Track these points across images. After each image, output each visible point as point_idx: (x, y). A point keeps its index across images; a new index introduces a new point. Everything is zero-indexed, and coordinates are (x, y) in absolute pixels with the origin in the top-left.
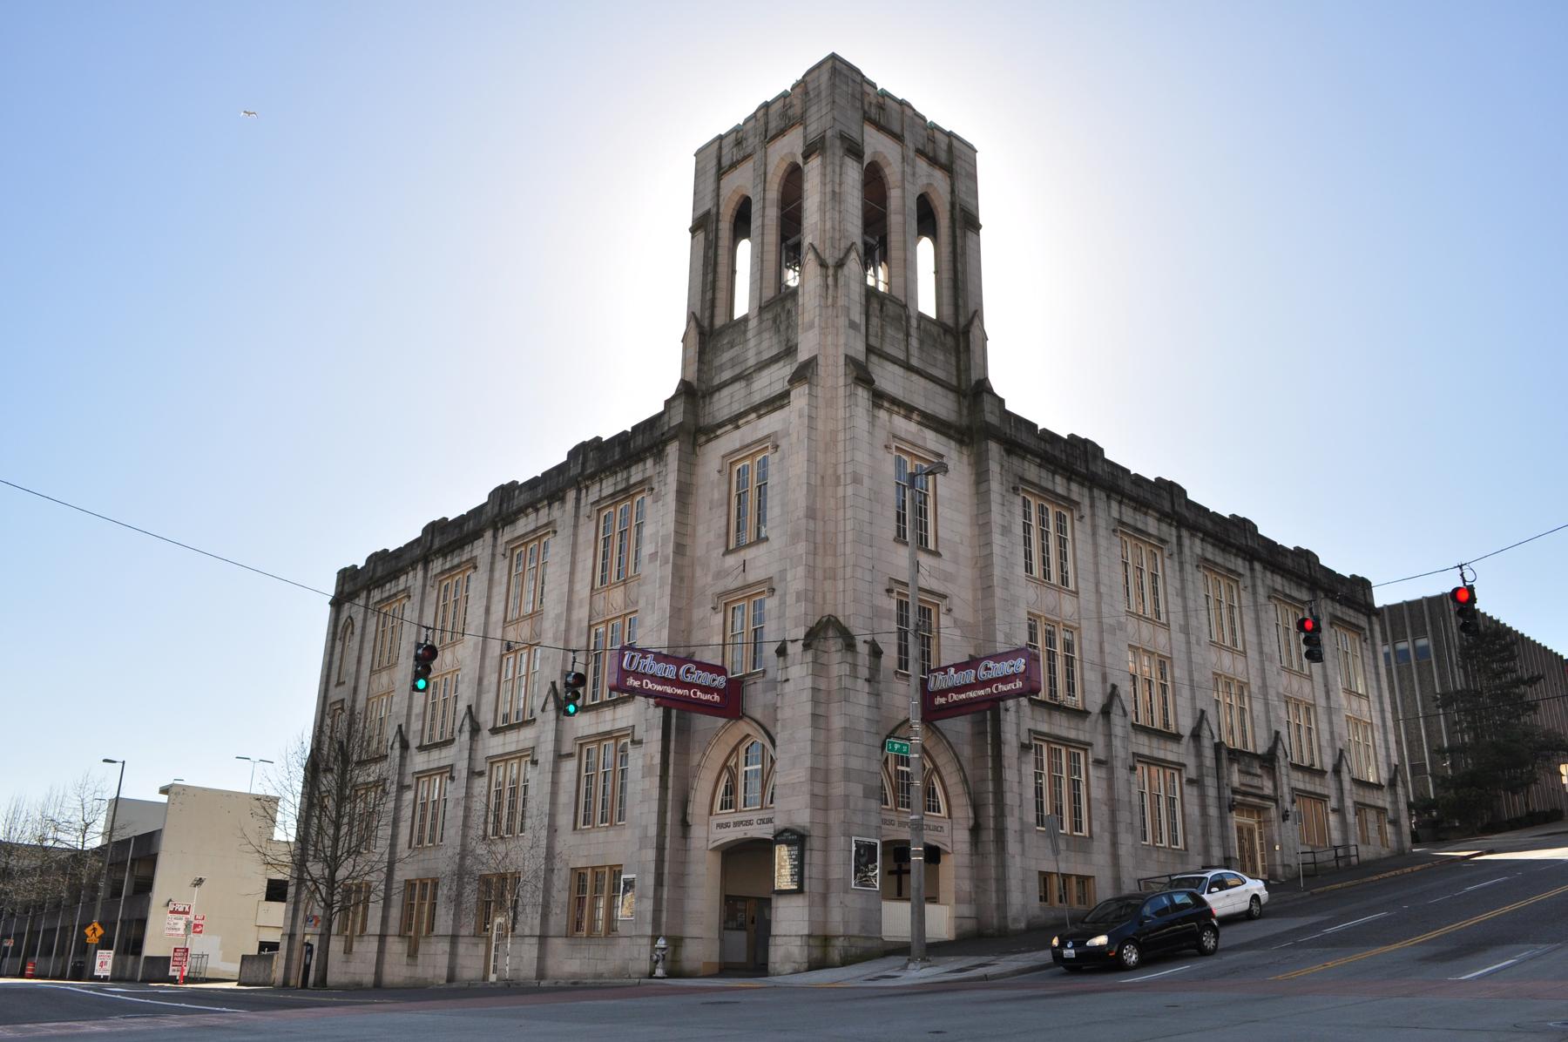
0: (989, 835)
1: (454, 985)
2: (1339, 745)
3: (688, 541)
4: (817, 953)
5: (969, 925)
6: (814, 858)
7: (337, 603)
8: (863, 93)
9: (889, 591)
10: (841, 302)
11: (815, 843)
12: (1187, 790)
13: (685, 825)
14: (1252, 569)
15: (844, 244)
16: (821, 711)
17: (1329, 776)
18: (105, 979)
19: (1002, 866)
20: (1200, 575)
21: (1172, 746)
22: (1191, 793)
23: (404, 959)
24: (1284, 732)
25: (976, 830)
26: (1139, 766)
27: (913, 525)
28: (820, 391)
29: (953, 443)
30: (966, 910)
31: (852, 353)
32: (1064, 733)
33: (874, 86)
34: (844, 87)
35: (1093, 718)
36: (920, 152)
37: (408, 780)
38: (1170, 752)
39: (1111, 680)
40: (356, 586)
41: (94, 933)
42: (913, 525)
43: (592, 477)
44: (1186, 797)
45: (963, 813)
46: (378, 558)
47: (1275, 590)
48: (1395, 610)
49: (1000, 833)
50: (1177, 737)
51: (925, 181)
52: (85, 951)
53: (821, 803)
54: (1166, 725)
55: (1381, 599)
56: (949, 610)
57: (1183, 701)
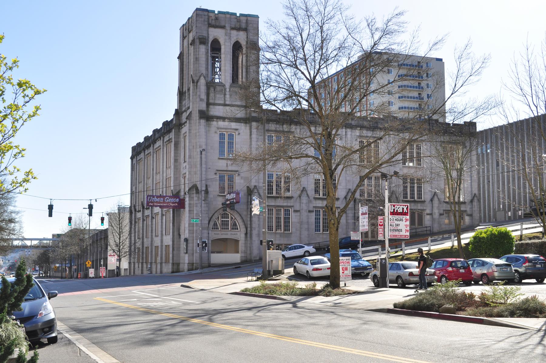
0: (248, 236)
1: (162, 275)
3: (178, 158)
4: (190, 267)
5: (244, 259)
6: (190, 245)
7: (132, 158)
8: (209, 17)
9: (216, 174)
10: (198, 93)
11: (190, 241)
13: (179, 235)
15: (199, 75)
16: (192, 209)
18: (93, 278)
19: (251, 243)
25: (246, 234)
28: (192, 122)
29: (243, 124)
30: (243, 255)
31: (201, 109)
32: (281, 204)
33: (213, 12)
34: (201, 20)
35: (295, 199)
36: (232, 29)
37: (145, 218)
40: (138, 151)
41: (89, 263)
43: (166, 133)
45: (243, 230)
46: (147, 138)
48: (481, 132)
49: (251, 235)
51: (235, 38)
52: (87, 269)
53: (191, 232)
55: (480, 128)
56: (239, 175)
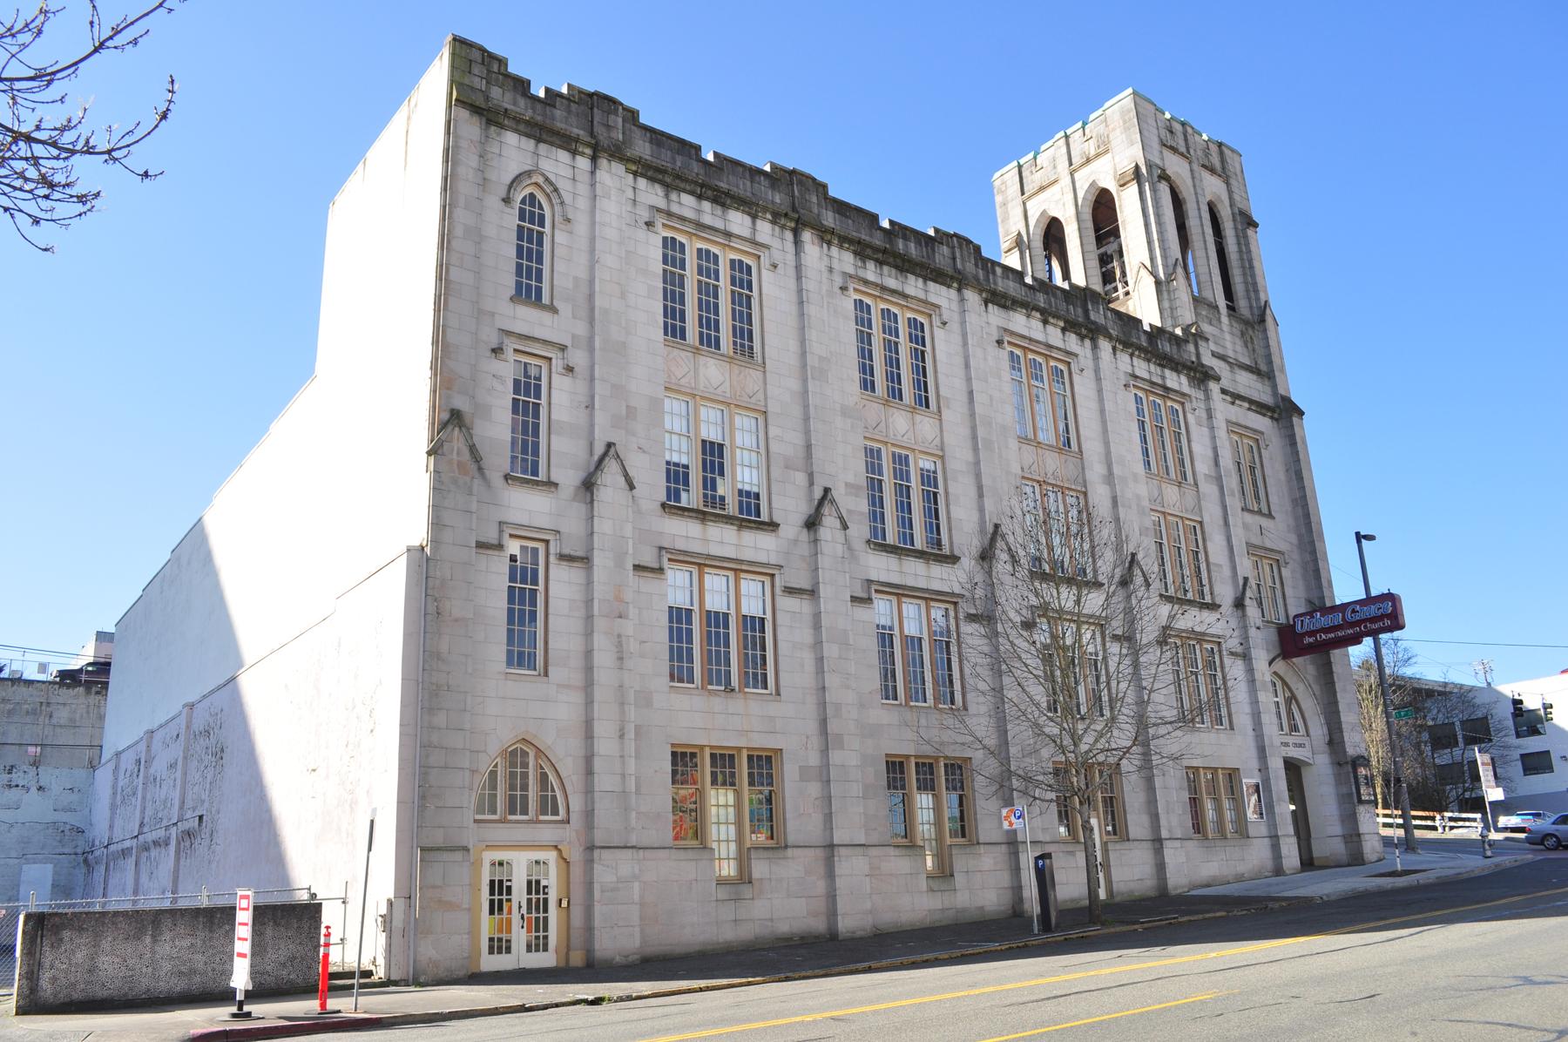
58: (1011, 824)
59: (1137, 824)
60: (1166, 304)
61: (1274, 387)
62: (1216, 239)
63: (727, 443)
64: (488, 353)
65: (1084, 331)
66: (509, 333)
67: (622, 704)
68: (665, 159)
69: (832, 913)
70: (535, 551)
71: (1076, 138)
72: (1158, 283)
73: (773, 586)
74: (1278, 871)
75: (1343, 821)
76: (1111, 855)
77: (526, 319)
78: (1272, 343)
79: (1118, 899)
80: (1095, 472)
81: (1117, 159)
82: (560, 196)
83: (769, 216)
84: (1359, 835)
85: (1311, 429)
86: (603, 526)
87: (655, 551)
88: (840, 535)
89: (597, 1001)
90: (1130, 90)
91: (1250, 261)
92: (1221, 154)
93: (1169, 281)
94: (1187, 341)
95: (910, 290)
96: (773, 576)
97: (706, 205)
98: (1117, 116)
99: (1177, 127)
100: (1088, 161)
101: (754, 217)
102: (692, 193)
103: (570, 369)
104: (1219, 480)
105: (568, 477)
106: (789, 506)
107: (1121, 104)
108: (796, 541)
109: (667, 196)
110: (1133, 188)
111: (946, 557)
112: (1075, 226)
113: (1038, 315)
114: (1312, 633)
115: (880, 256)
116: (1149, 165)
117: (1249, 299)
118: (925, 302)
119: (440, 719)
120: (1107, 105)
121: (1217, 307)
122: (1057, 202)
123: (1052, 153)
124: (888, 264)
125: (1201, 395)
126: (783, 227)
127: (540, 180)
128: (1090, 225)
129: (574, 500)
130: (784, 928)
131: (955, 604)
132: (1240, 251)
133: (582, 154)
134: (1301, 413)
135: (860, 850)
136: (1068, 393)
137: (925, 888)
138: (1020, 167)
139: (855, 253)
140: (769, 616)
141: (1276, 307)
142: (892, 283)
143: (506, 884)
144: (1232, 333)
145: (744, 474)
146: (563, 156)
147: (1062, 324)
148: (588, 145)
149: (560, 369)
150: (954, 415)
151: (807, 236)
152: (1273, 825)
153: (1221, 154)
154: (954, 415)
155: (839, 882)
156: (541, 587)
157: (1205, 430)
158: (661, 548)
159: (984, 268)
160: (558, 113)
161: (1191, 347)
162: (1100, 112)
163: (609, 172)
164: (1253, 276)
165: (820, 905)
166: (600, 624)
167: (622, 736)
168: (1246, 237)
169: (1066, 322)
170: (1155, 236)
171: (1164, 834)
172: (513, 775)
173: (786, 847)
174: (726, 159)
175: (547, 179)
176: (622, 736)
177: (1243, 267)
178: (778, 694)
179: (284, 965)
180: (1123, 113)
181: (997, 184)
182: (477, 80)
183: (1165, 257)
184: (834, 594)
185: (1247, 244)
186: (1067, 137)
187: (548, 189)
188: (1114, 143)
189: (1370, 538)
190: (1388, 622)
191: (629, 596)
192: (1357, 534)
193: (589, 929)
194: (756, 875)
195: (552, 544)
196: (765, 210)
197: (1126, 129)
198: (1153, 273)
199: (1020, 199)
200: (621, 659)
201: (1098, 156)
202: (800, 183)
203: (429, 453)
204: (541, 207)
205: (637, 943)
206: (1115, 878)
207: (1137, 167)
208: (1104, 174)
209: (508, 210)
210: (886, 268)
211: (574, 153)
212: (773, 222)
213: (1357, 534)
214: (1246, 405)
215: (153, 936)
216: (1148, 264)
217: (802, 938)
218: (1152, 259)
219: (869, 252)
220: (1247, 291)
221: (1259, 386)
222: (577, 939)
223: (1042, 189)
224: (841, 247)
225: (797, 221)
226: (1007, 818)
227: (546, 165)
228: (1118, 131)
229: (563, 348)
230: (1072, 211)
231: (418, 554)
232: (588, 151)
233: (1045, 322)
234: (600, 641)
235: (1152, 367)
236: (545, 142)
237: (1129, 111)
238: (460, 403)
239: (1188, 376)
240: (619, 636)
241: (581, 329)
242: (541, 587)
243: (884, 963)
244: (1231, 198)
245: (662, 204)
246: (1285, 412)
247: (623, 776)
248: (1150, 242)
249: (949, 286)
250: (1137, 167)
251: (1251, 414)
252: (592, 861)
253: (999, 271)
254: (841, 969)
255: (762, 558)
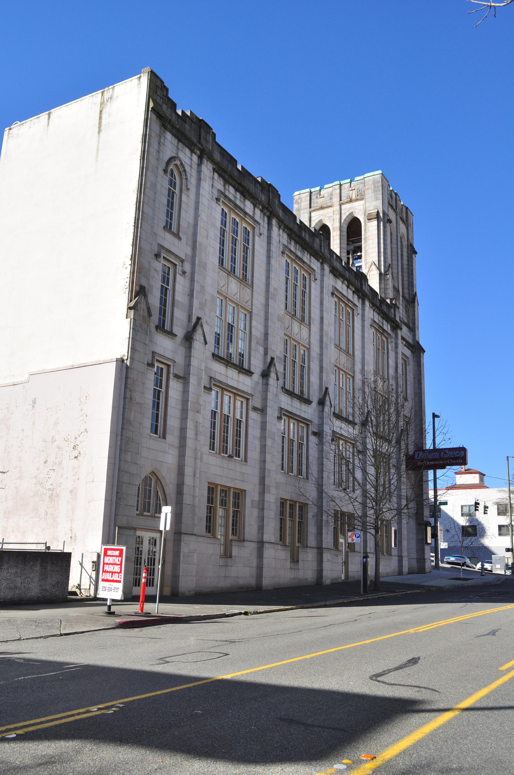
2: (196, 314)
12: (253, 415)
14: (323, 269)
17: (314, 404)
20: (283, 260)
21: (304, 407)
22: (313, 440)
23: (288, 564)
24: (331, 390)
26: (284, 417)
27: (299, 313)
38: (244, 383)
39: (270, 354)
42: (299, 313)
44: (310, 444)
47: (375, 322)
50: (308, 402)
54: (302, 392)
57: (314, 379)
58: (353, 540)
59: (312, 541)
60: (383, 286)
61: (414, 336)
62: (402, 257)
63: (235, 325)
64: (153, 256)
65: (360, 295)
66: (163, 247)
67: (196, 458)
68: (225, 164)
69: (260, 575)
70: (162, 369)
71: (345, 187)
72: (380, 274)
73: (247, 405)
74: (400, 573)
75: (417, 552)
76: (349, 559)
77: (168, 241)
78: (416, 314)
79: (350, 580)
80: (358, 367)
81: (367, 205)
82: (186, 175)
83: (261, 207)
84: (424, 559)
85: (427, 359)
86: (194, 362)
87: (209, 378)
88: (275, 381)
89: (246, 613)
90: (380, 172)
91: (412, 271)
92: (407, 213)
93: (386, 274)
94: (392, 307)
95: (305, 260)
96: (248, 399)
97: (238, 195)
98: (371, 183)
99: (394, 195)
100: (351, 201)
101: (255, 206)
102: (234, 187)
103: (184, 273)
104: (396, 378)
105: (179, 331)
106: (257, 365)
107: (374, 176)
108: (258, 383)
109: (224, 186)
110: (375, 223)
111: (305, 399)
112: (338, 233)
113: (346, 283)
114: (422, 461)
115: (297, 238)
116: (384, 213)
117: (409, 290)
118: (309, 266)
119: (128, 457)
120: (366, 175)
121: (399, 291)
122: (329, 217)
123: (330, 190)
124: (299, 244)
125: (393, 335)
126: (264, 214)
127: (178, 163)
128: (345, 234)
129: (181, 345)
130: (241, 582)
131: (308, 425)
132: (408, 265)
133: (195, 153)
134: (424, 352)
135: (272, 545)
136: (351, 325)
137: (289, 567)
138: (311, 193)
139: (289, 235)
140: (244, 420)
141: (420, 297)
142: (299, 254)
143: (141, 549)
144: (402, 305)
145: (240, 345)
146: (188, 152)
147: (354, 289)
148: (199, 149)
149: (180, 272)
150: (315, 327)
151: (274, 222)
152: (400, 551)
153: (407, 213)
154: (315, 327)
155: (265, 561)
156: (163, 390)
157: (394, 353)
158: (211, 378)
159: (330, 254)
160: (187, 126)
161: (393, 311)
162: (362, 177)
163: (207, 167)
164: (412, 279)
165: (254, 571)
166: (190, 414)
167: (194, 476)
168: (412, 258)
169: (355, 288)
170: (382, 250)
171: (368, 551)
172: (145, 490)
173: (244, 540)
174: (247, 171)
175: (182, 164)
176: (194, 476)
177: (408, 273)
178: (246, 461)
179: (54, 586)
180: (374, 182)
181: (296, 198)
182: (159, 98)
183: (385, 262)
184: (272, 413)
185: (412, 262)
186: (341, 185)
187: (181, 169)
188: (367, 196)
189: (438, 416)
190: (461, 461)
191: (201, 402)
192: (434, 414)
193: (175, 576)
194: (234, 554)
195: (172, 367)
196: (260, 203)
197: (375, 191)
198: (379, 268)
199: (308, 210)
200: (196, 434)
201: (357, 200)
202: (273, 193)
203: (130, 308)
204: (175, 179)
205: (194, 586)
206: (350, 570)
207: (378, 212)
208: (358, 209)
209: (165, 177)
210: (298, 245)
211: (192, 152)
212: (261, 211)
213: (434, 414)
214: (404, 343)
215: (31, 566)
216: (377, 263)
217: (247, 588)
218: (379, 261)
219: (293, 236)
220: (409, 285)
221: (408, 334)
222: (168, 581)
223: (322, 208)
224: (284, 230)
225: (271, 213)
226: (350, 537)
227: (181, 155)
228: (370, 191)
229: (182, 261)
230: (337, 225)
231: (120, 363)
232: (198, 152)
233: (348, 287)
234: (190, 424)
235: (380, 317)
236: (182, 142)
237: (378, 182)
238: (144, 282)
239: (391, 325)
240: (197, 422)
241: (188, 251)
242: (163, 390)
243: (328, 603)
244: (408, 237)
245: (222, 190)
246: (417, 350)
247: (194, 496)
248: (379, 252)
249: (318, 261)
250: (378, 212)
251: (405, 348)
252: (180, 540)
253: (335, 256)
254: (332, 602)
255: (245, 389)
